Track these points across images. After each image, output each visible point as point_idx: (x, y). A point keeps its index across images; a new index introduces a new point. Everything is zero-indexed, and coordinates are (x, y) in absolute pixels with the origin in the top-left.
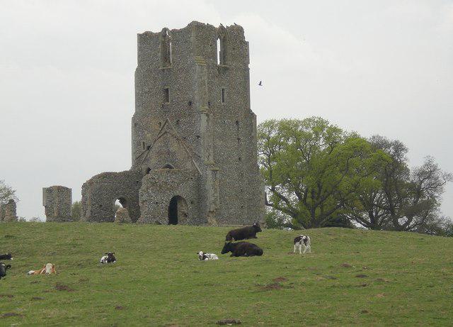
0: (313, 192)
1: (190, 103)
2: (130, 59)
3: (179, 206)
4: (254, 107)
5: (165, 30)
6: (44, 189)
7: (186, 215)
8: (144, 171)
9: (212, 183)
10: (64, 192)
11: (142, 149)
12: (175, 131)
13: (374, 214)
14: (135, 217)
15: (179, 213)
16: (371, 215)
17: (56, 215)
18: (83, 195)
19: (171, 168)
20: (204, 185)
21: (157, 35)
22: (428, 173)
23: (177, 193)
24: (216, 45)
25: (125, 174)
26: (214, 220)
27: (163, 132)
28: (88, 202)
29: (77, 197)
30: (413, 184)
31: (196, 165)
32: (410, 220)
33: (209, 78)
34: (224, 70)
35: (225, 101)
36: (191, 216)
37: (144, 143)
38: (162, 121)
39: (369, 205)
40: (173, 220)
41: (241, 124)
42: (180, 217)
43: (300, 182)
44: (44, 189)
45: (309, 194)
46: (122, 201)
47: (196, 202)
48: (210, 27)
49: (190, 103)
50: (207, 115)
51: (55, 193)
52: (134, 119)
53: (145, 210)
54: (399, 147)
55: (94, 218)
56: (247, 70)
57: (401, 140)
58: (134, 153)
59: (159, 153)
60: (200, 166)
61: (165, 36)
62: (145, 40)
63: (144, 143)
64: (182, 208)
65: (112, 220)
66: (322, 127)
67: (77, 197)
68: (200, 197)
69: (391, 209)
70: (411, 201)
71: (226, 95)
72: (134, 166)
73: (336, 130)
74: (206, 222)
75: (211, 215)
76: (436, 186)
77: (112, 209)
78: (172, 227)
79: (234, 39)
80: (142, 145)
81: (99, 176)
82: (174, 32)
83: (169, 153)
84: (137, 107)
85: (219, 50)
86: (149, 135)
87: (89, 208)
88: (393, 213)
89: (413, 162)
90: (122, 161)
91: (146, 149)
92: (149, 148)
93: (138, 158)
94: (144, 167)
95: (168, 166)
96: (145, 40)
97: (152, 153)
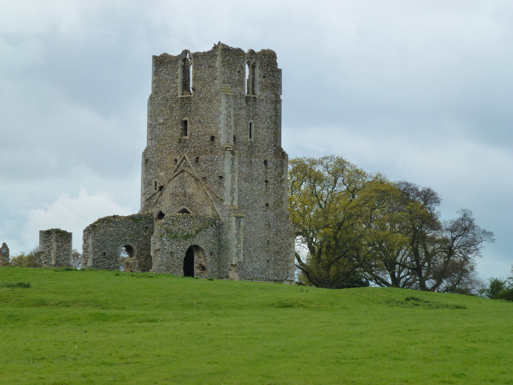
0: (328, 247)
1: (213, 138)
3: (196, 257)
5: (186, 52)
6: (41, 232)
7: (203, 268)
8: (155, 216)
9: (235, 231)
12: (193, 170)
13: (396, 274)
15: (195, 265)
16: (393, 276)
17: (53, 262)
19: (187, 212)
20: (225, 234)
23: (195, 242)
24: (245, 72)
25: (132, 218)
27: (179, 170)
28: (90, 249)
31: (218, 209)
32: (439, 282)
33: (235, 109)
35: (253, 136)
36: (209, 270)
37: (156, 182)
38: (178, 158)
40: (189, 271)
42: (197, 271)
43: (133, 232)
44: (41, 232)
45: (324, 249)
47: (215, 252)
48: (238, 52)
49: (213, 138)
50: (233, 153)
52: (145, 154)
55: (97, 266)
57: (434, 189)
58: (143, 194)
59: (174, 195)
63: (156, 182)
64: (198, 260)
69: (417, 270)
71: (253, 131)
72: (143, 209)
73: (359, 173)
75: (233, 269)
77: (115, 256)
80: (154, 184)
81: (101, 221)
83: (185, 195)
84: (150, 140)
85: (247, 77)
86: (162, 174)
87: (91, 256)
88: (420, 274)
91: (158, 189)
92: (161, 188)
94: (155, 211)
95: (184, 211)
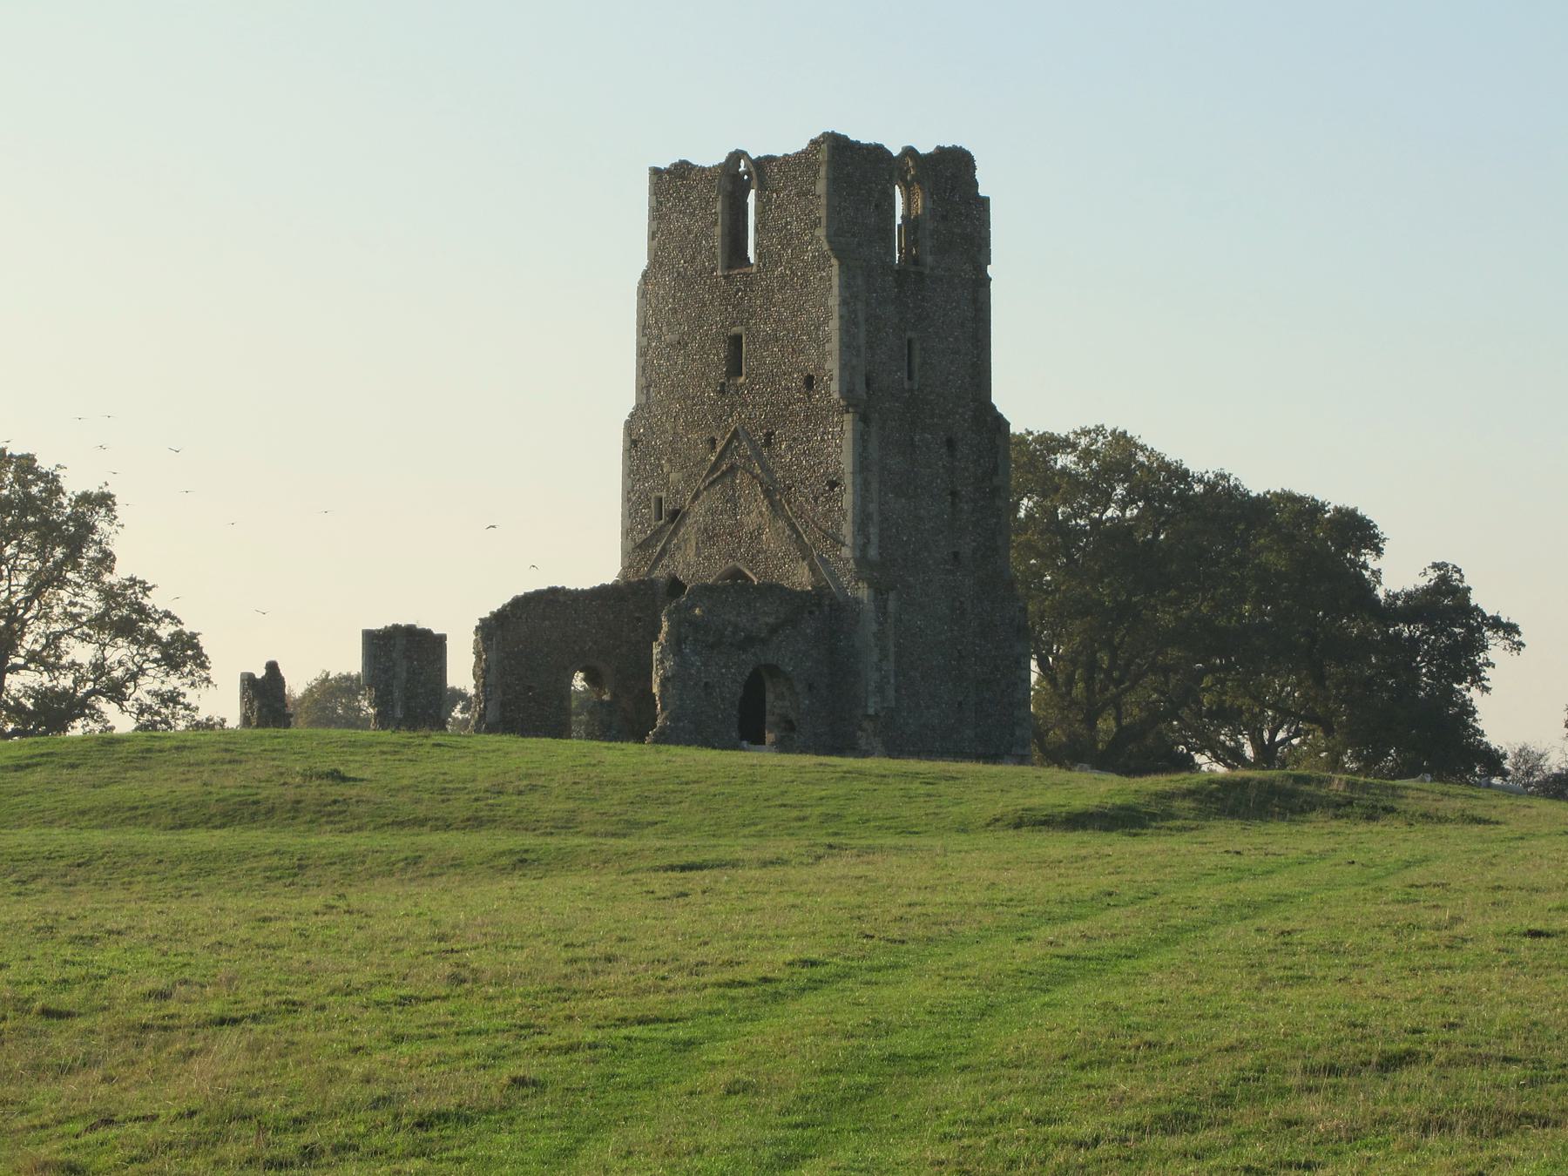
1: (809, 381)
4: (1002, 398)
25: (601, 593)
29: (461, 672)
34: (911, 276)
48: (878, 151)
49: (809, 381)
52: (630, 426)
58: (627, 533)
61: (737, 177)
64: (774, 704)
67: (461, 672)
82: (763, 165)
97: (690, 531)
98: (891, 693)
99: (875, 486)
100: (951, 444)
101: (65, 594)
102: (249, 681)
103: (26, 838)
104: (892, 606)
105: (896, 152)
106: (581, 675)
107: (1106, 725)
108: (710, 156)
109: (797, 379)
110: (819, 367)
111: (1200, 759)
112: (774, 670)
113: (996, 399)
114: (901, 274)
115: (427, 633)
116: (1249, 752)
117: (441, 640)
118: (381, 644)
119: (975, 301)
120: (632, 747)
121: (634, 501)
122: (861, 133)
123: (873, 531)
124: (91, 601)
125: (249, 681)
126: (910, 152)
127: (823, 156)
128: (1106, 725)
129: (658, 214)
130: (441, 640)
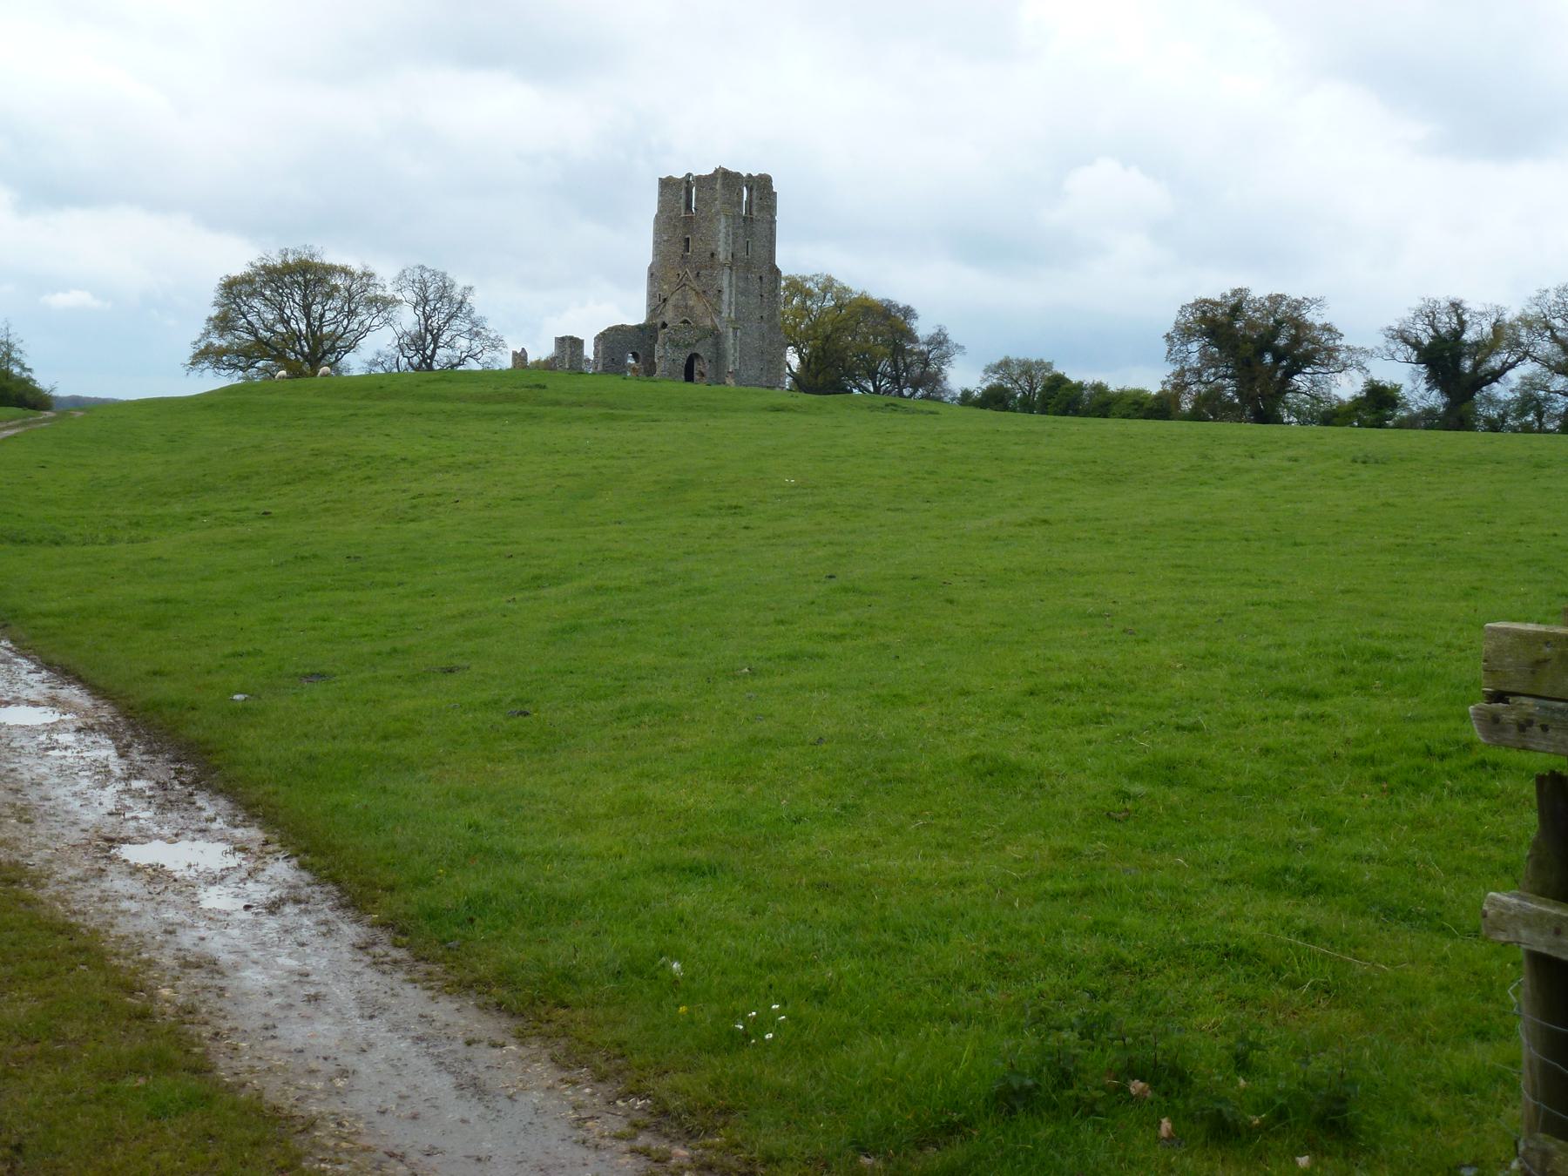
1: (712, 255)
2: (649, 205)
4: (780, 262)
7: (702, 375)
8: (659, 325)
10: (576, 344)
11: (657, 302)
12: (694, 284)
14: (650, 370)
16: (874, 385)
18: (595, 347)
19: (688, 322)
21: (680, 181)
22: (939, 340)
25: (638, 327)
26: (732, 381)
29: (589, 351)
30: (921, 353)
31: (717, 321)
32: (916, 391)
34: (748, 220)
36: (708, 376)
39: (872, 375)
40: (689, 377)
41: (765, 280)
42: (696, 377)
45: (813, 360)
46: (635, 356)
48: (738, 175)
49: (712, 255)
50: (731, 268)
51: (568, 342)
52: (650, 268)
53: (661, 366)
54: (908, 312)
56: (774, 222)
57: (913, 306)
58: (648, 306)
59: (676, 307)
60: (720, 323)
61: (688, 182)
62: (667, 184)
64: (697, 367)
65: (1472, 428)
66: (831, 286)
67: (589, 351)
68: (719, 357)
69: (895, 379)
70: (917, 371)
74: (724, 383)
75: (729, 375)
76: (944, 358)
78: (689, 385)
79: (762, 187)
82: (699, 178)
83: (686, 307)
84: (655, 255)
87: (601, 361)
88: (898, 383)
89: (923, 328)
90: (633, 312)
92: (665, 300)
93: (653, 311)
94: (659, 322)
96: (667, 184)
97: (669, 306)
98: (737, 364)
99: (734, 292)
100: (761, 278)
101: (458, 322)
102: (515, 354)
103: (1561, 705)
104: (738, 334)
105: (744, 175)
106: (1467, 371)
107: (820, 379)
108: (680, 175)
109: (708, 254)
110: (716, 250)
111: (854, 390)
112: (697, 355)
113: (777, 263)
114: (745, 219)
115: (577, 339)
116: (872, 389)
117: (582, 341)
118: (562, 342)
119: (771, 228)
120: (1235, 425)
121: (652, 295)
122: (732, 168)
123: (733, 308)
124: (466, 326)
125: (515, 354)
126: (750, 176)
127: (719, 176)
128: (820, 379)
129: (661, 194)
130: (582, 341)
